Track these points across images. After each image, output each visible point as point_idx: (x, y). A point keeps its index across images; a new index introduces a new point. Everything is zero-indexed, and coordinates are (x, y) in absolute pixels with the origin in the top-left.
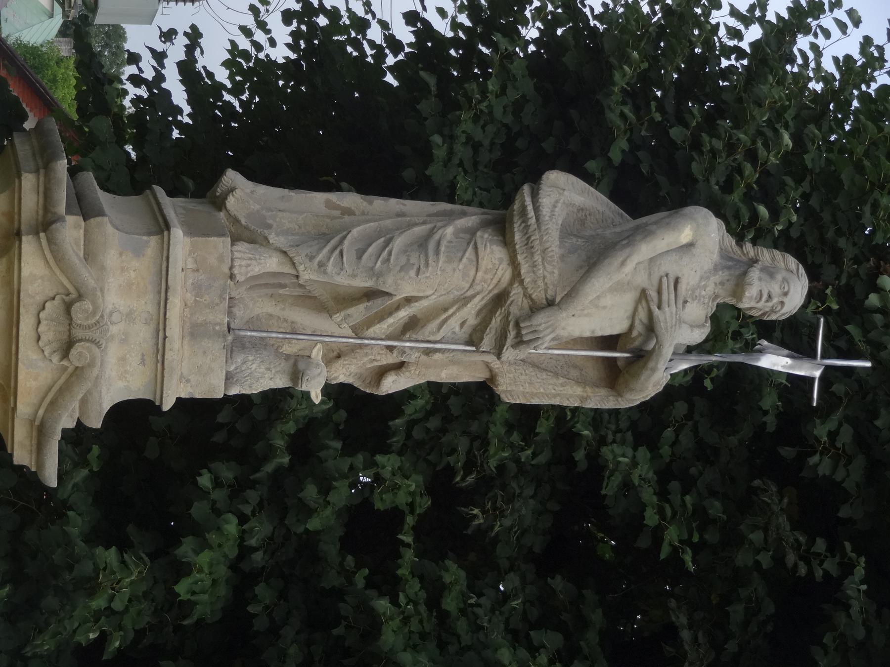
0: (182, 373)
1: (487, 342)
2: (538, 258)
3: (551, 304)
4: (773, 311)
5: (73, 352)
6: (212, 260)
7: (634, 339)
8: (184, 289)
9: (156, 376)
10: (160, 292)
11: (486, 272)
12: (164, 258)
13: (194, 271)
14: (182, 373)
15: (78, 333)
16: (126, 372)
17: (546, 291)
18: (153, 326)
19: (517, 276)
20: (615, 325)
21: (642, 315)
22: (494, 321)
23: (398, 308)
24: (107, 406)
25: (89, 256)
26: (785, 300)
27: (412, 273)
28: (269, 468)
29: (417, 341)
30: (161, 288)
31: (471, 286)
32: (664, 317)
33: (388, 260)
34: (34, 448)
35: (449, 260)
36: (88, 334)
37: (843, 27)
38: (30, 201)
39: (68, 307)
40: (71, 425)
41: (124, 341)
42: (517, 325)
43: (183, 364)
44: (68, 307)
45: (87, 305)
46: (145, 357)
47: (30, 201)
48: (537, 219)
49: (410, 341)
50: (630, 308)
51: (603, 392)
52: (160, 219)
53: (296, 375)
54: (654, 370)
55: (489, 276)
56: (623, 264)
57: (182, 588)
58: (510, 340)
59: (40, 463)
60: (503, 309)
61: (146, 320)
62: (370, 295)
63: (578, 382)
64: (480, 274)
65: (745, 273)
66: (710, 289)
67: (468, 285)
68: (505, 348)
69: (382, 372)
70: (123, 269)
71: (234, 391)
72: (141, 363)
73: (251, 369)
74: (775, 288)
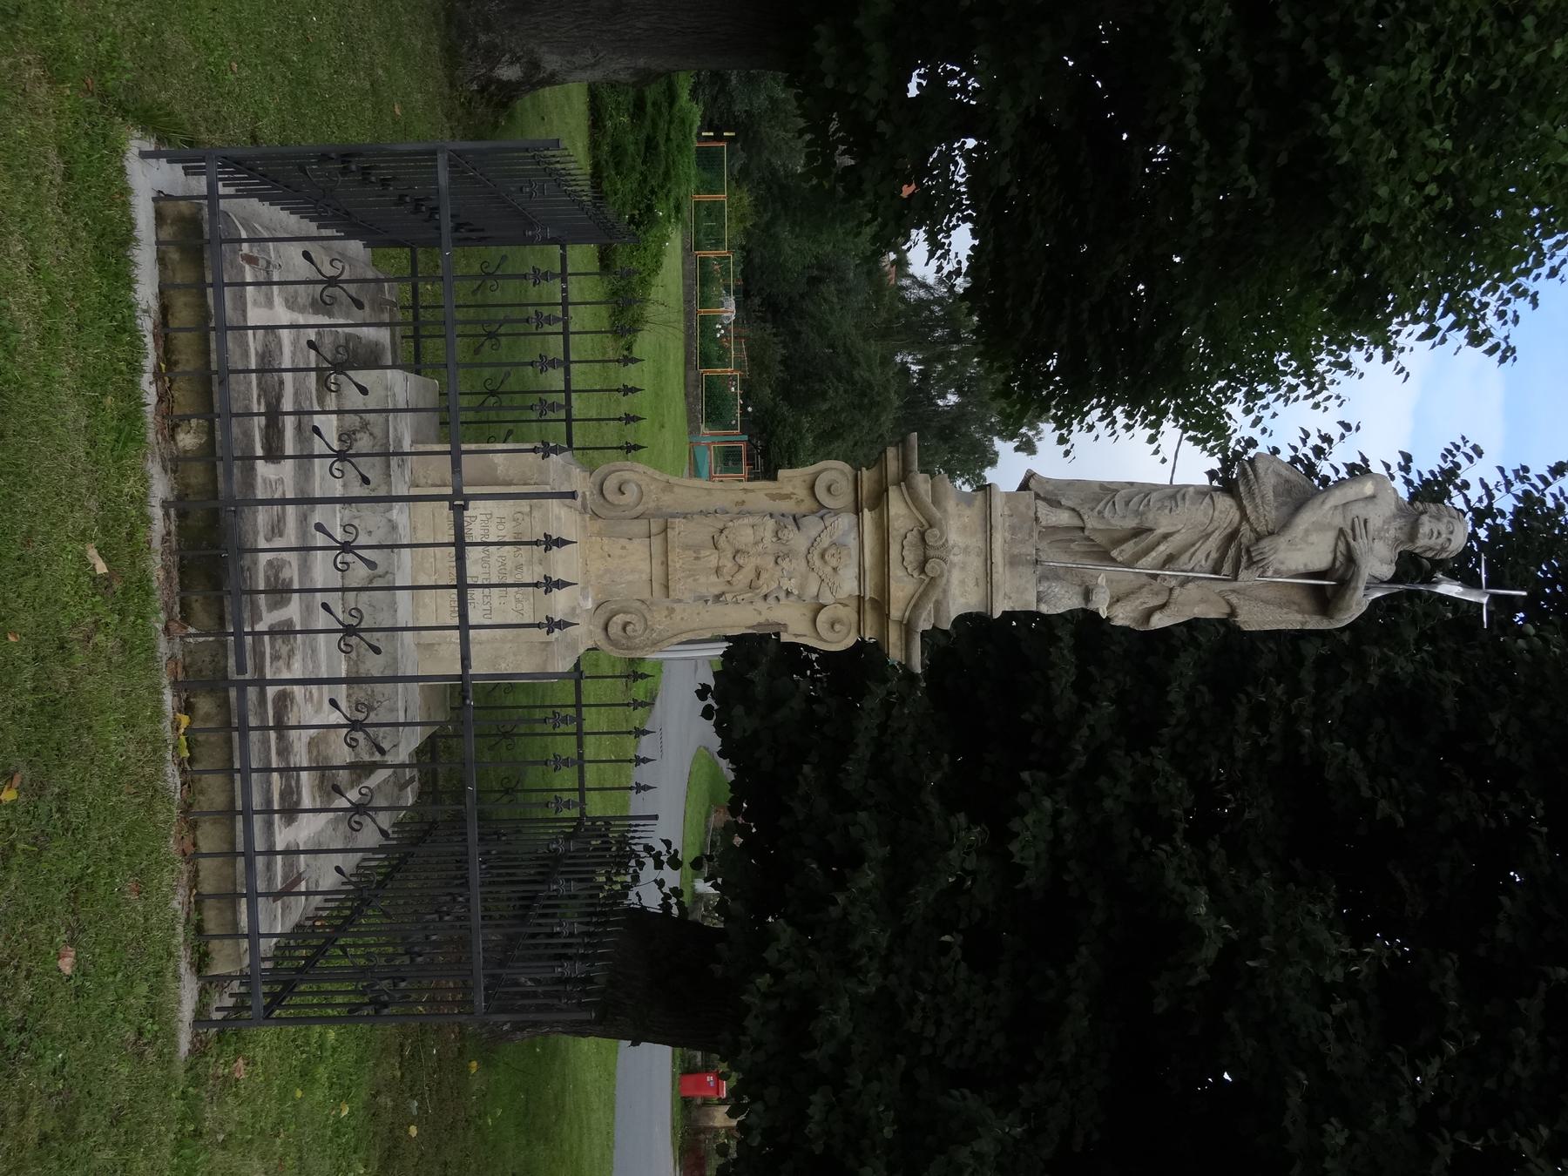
1: (1227, 568)
2: (1258, 500)
3: (1271, 534)
4: (1443, 549)
5: (928, 566)
6: (1022, 508)
7: (1338, 570)
11: (1221, 512)
15: (931, 553)
16: (966, 591)
17: (1267, 526)
18: (983, 557)
19: (1244, 516)
20: (1321, 560)
21: (1342, 547)
23: (1158, 544)
24: (953, 616)
25: (936, 501)
26: (1452, 537)
27: (1167, 511)
28: (1072, 767)
29: (1174, 571)
31: (1211, 522)
32: (1360, 546)
33: (1148, 504)
34: (903, 647)
35: (1193, 503)
36: (937, 553)
37: (1470, 459)
38: (893, 466)
39: (922, 536)
40: (929, 627)
41: (963, 568)
42: (1248, 551)
44: (922, 536)
45: (936, 531)
47: (893, 466)
48: (1255, 476)
49: (1168, 570)
51: (1318, 618)
53: (1087, 594)
54: (1356, 589)
55: (1223, 516)
56: (1323, 502)
57: (1014, 847)
59: (908, 657)
62: (1138, 532)
63: (1298, 612)
64: (1216, 513)
65: (1417, 520)
66: (1392, 533)
67: (1208, 522)
69: (1149, 614)
70: (959, 516)
71: (1044, 609)
74: (1443, 527)
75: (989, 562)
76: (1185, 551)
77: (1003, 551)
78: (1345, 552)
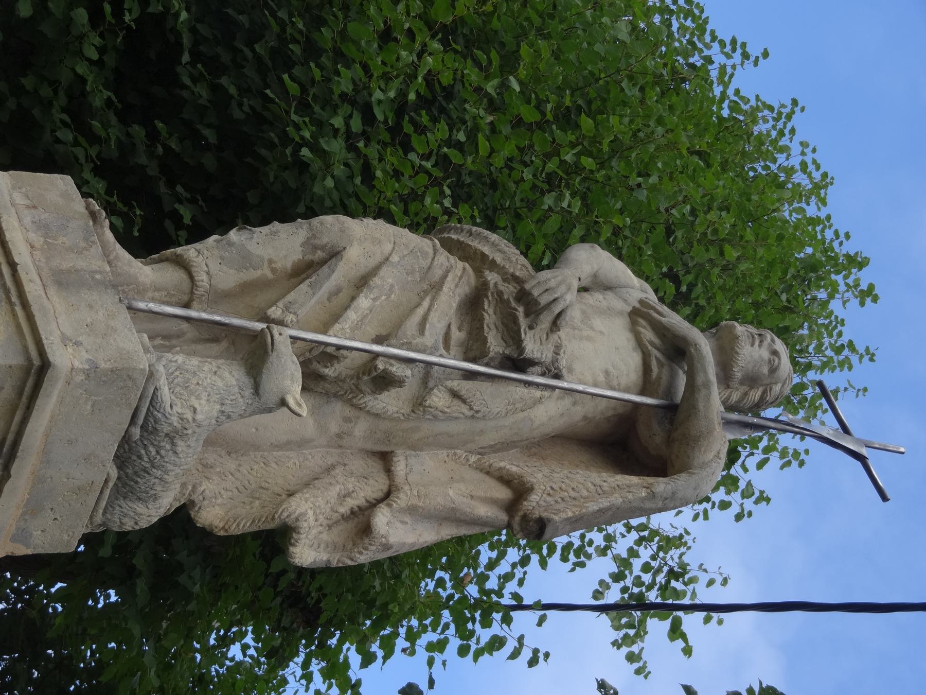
9: (18, 326)
10: (20, 394)
13: (28, 207)
14: (63, 334)
21: (648, 335)
43: (60, 321)
52: (14, 427)
58: (523, 322)
60: (490, 295)
73: (176, 361)
78: (657, 341)
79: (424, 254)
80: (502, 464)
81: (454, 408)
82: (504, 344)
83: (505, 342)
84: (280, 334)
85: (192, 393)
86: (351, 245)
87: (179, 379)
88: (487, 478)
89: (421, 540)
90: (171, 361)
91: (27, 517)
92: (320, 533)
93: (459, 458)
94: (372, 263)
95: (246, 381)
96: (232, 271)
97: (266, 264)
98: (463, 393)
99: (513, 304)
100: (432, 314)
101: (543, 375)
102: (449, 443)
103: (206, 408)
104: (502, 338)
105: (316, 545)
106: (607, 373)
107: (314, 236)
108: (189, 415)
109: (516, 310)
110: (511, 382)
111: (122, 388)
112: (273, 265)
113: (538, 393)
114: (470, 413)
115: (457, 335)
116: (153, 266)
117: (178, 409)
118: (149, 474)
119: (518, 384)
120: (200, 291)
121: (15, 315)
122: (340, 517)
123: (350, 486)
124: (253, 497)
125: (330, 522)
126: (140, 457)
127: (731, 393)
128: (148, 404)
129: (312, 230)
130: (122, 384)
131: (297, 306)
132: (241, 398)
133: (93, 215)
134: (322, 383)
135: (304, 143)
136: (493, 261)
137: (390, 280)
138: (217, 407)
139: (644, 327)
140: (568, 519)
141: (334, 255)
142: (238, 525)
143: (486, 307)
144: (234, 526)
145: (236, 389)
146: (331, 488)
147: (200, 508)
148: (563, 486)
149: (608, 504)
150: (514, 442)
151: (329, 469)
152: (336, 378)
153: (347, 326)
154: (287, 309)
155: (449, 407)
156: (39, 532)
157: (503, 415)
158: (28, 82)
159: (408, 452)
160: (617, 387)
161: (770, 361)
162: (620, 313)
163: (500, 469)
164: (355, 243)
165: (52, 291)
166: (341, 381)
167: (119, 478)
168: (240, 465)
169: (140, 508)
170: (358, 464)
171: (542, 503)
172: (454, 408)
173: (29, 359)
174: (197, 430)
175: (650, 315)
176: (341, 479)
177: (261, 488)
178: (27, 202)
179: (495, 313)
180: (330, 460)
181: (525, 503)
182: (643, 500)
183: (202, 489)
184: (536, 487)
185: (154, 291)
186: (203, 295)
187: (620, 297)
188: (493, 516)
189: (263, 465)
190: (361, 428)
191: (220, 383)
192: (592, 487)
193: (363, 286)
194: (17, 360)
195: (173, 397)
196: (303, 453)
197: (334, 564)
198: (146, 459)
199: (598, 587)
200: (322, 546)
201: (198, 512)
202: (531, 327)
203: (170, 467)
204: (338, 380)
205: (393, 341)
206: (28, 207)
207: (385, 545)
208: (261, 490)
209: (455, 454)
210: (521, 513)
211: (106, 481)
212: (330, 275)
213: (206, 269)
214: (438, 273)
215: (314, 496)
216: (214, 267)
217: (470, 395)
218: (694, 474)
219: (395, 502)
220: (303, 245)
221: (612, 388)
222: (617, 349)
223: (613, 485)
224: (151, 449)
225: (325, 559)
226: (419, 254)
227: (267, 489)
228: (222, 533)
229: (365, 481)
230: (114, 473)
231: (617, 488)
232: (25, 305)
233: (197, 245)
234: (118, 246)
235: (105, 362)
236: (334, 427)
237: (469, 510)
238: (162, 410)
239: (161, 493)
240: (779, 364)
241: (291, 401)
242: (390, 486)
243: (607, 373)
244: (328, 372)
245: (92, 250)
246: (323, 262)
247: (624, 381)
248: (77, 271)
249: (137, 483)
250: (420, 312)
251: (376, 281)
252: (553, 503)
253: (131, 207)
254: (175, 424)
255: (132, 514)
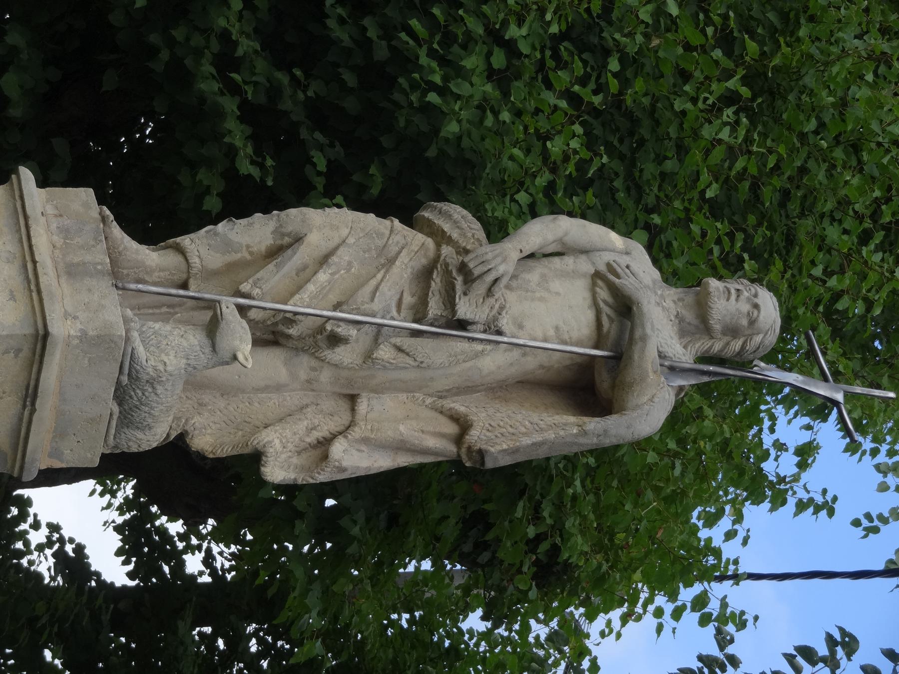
0: (65, 310)
8: (49, 233)
9: (33, 307)
12: (17, 197)
13: (56, 216)
14: (65, 310)
18: (18, 263)
21: (603, 294)
22: (433, 283)
30: (21, 235)
43: (65, 301)
46: (15, 293)
50: (587, 295)
52: (33, 376)
60: (439, 266)
61: (8, 259)
68: (457, 296)
72: (10, 299)
75: (30, 266)
76: (363, 285)
77: (53, 259)
78: (610, 300)
79: (380, 235)
80: (452, 405)
81: (399, 360)
82: (444, 308)
83: (445, 306)
84: (227, 307)
85: (162, 351)
86: (311, 232)
87: (153, 341)
88: (440, 417)
89: (376, 465)
90: (150, 328)
91: (57, 440)
92: (290, 457)
93: (417, 400)
94: (332, 245)
95: (206, 342)
96: (218, 255)
97: (244, 248)
98: (404, 348)
99: (454, 274)
100: (383, 284)
101: (485, 332)
102: (408, 388)
103: (175, 362)
104: (443, 303)
105: (286, 466)
106: (557, 328)
107: (281, 226)
108: (161, 368)
109: (456, 279)
110: (452, 338)
111: (108, 348)
112: (250, 249)
113: (479, 347)
114: (417, 364)
115: (408, 299)
116: (160, 252)
117: (152, 362)
118: (139, 409)
119: (461, 339)
120: (194, 271)
121: (32, 299)
122: (308, 446)
123: (316, 422)
124: (238, 429)
125: (297, 449)
126: (131, 397)
127: (714, 343)
128: (129, 359)
129: (279, 221)
130: (107, 346)
131: (262, 282)
132: (204, 356)
133: (104, 219)
134: (291, 340)
135: (433, 87)
136: (450, 237)
137: (347, 258)
138: (184, 361)
139: (601, 288)
140: (504, 451)
141: (298, 239)
142: (223, 450)
143: (434, 277)
144: (219, 451)
145: (198, 348)
146: (300, 423)
147: (192, 436)
148: (502, 424)
149: (541, 439)
150: (469, 387)
151: (302, 408)
152: (299, 336)
153: (306, 296)
154: (255, 284)
155: (394, 359)
156: (69, 451)
157: (447, 365)
158: (179, 34)
159: (372, 395)
160: (568, 340)
161: (748, 313)
162: (584, 275)
163: (450, 409)
164: (315, 230)
165: (63, 280)
166: (303, 339)
167: (120, 412)
168: (229, 404)
169: (139, 435)
170: (328, 404)
171: (482, 437)
172: (399, 360)
173: (37, 330)
174: (170, 378)
175: (607, 277)
176: (309, 416)
177: (246, 422)
178: (56, 212)
179: (441, 282)
180: (306, 401)
181: (467, 437)
182: (576, 435)
183: (193, 422)
184: (475, 424)
185: (159, 271)
186: (197, 274)
187: (590, 260)
188: (441, 447)
189: (247, 404)
190: (325, 376)
191: (185, 344)
192: (530, 425)
193: (324, 263)
194: (29, 331)
195: (148, 354)
196: (283, 395)
197: (300, 482)
198: (136, 399)
199: (894, 557)
200: (292, 467)
201: (191, 439)
202: (465, 294)
203: (155, 405)
204: (300, 338)
205: (345, 307)
206: (56, 216)
207: (338, 467)
208: (245, 424)
209: (414, 397)
210: (466, 446)
211: (111, 415)
212: (292, 256)
213: (197, 254)
214: (394, 249)
215: (283, 429)
216: (204, 251)
217: (412, 349)
218: (625, 414)
219: (350, 434)
220: (273, 233)
221: (565, 343)
222: (570, 307)
223: (549, 423)
224: (138, 391)
225: (293, 477)
226: (374, 235)
227: (249, 423)
228: (211, 456)
229: (330, 417)
230: (116, 409)
231: (553, 425)
232: (39, 292)
233: (192, 236)
234: (127, 239)
235: (93, 331)
236: (303, 375)
237: (417, 442)
238: (139, 364)
239: (153, 424)
240: (758, 316)
241: (240, 357)
242: (351, 422)
243: (557, 328)
244: (293, 331)
245: (99, 247)
246: (290, 246)
247: (575, 335)
248: (84, 264)
249: (132, 416)
250: (373, 283)
251: (335, 259)
252: (493, 437)
253: (264, 159)
254: (151, 373)
255: (134, 439)
